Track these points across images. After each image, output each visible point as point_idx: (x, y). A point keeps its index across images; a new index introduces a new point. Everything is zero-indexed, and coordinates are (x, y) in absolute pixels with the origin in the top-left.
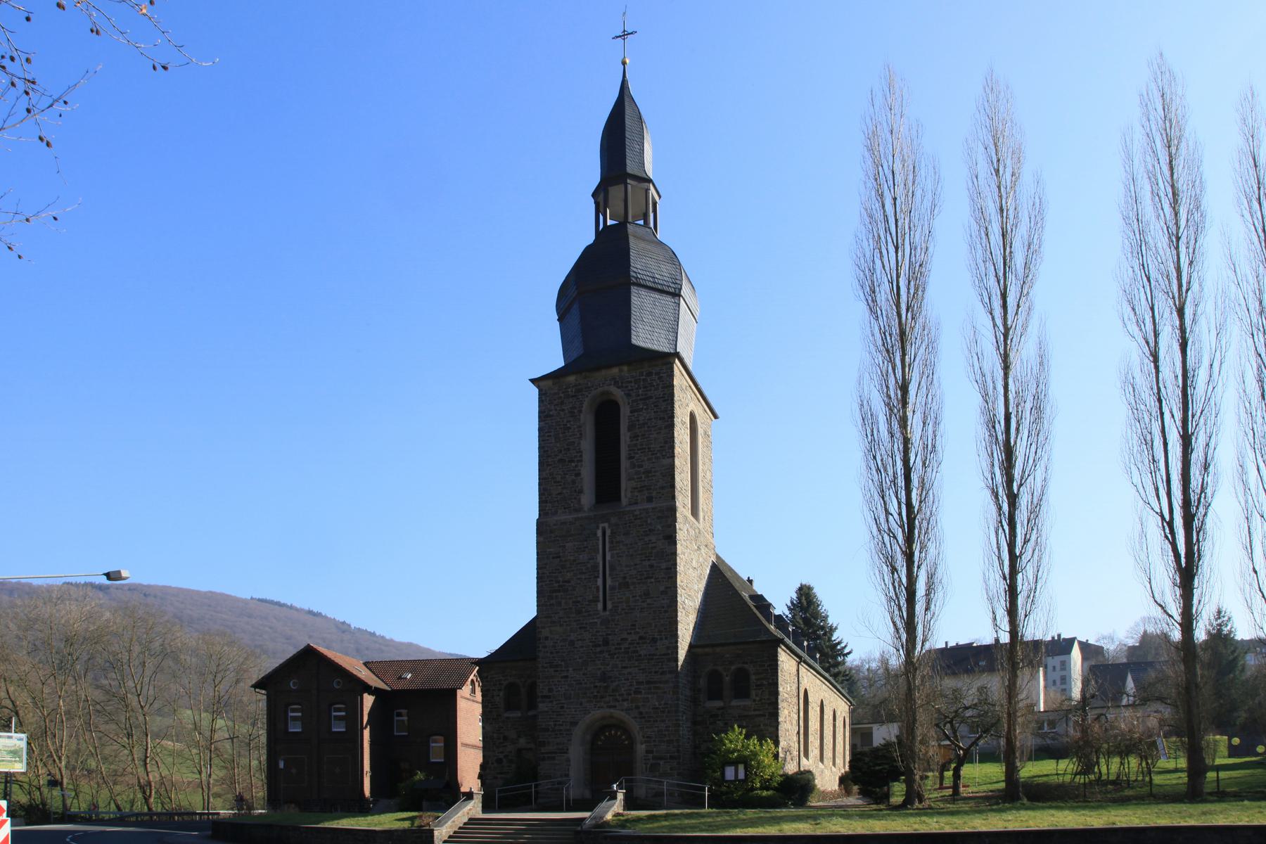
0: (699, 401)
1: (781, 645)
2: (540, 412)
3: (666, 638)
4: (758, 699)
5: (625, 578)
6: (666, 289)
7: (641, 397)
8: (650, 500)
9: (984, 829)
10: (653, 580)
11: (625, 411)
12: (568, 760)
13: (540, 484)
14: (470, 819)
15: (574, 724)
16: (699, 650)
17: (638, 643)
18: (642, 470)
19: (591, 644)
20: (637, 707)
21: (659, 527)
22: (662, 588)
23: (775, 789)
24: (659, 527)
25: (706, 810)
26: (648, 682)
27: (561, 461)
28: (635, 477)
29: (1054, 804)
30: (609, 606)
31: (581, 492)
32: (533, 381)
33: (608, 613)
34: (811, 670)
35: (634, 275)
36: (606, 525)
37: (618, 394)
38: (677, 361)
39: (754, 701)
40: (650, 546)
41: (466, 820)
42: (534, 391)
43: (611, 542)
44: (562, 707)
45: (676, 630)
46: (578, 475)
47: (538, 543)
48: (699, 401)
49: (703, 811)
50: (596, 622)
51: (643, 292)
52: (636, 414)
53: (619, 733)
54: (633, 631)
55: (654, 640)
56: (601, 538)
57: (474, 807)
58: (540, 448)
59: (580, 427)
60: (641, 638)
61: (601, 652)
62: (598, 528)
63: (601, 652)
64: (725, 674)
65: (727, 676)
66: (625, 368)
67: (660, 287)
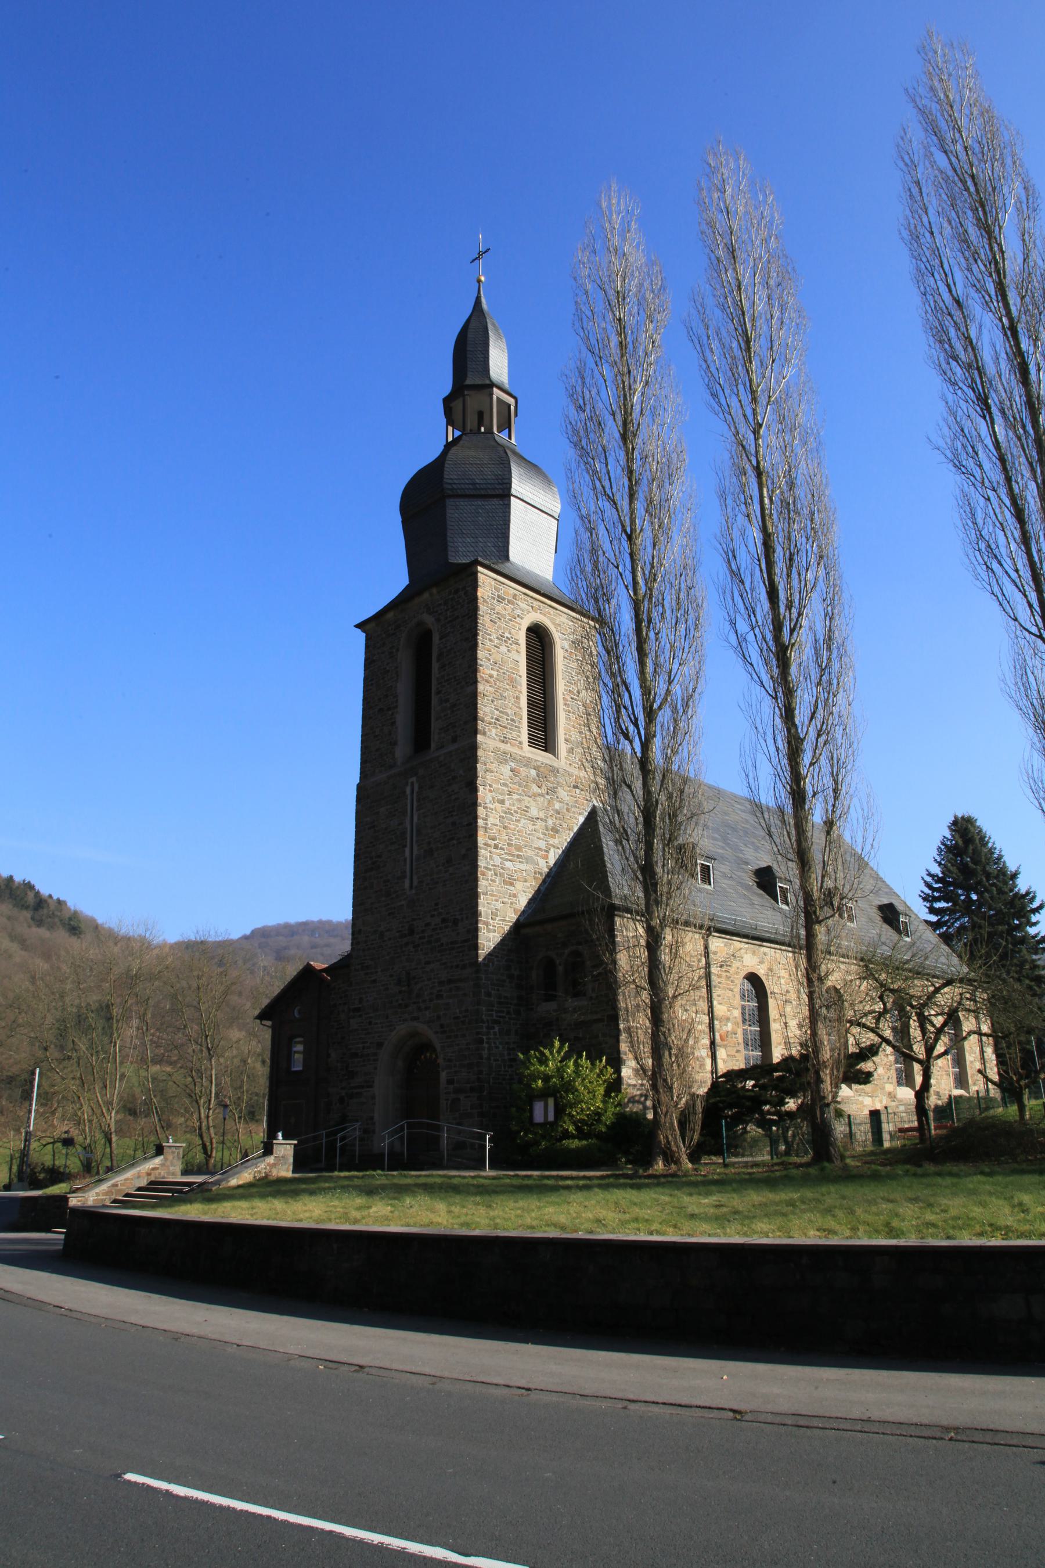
0: (556, 609)
1: (616, 913)
2: (366, 660)
3: (467, 918)
4: (594, 995)
5: (429, 843)
6: (490, 492)
7: (449, 619)
8: (454, 740)
9: (394, 1228)
10: (455, 842)
11: (436, 638)
12: (373, 1097)
13: (363, 742)
14: (151, 1183)
15: (380, 1045)
16: (525, 931)
17: (441, 929)
18: (448, 705)
19: (397, 934)
20: (439, 1017)
21: (461, 772)
22: (463, 851)
23: (599, 1136)
24: (461, 772)
25: (489, 1173)
26: (450, 981)
27: (381, 710)
28: (442, 715)
29: (437, 1176)
30: (415, 883)
31: (395, 743)
32: (358, 626)
33: (414, 891)
34: (765, 944)
35: (450, 487)
36: (414, 779)
37: (429, 620)
38: (480, 568)
39: (591, 998)
40: (453, 797)
41: (143, 1183)
42: (361, 637)
43: (418, 800)
44: (370, 1023)
45: (476, 905)
46: (393, 723)
47: (357, 813)
48: (556, 609)
49: (483, 1173)
50: (403, 905)
51: (462, 503)
52: (444, 640)
53: (428, 1055)
54: (436, 913)
55: (455, 922)
56: (409, 797)
57: (162, 1165)
58: (364, 700)
59: (397, 667)
60: (444, 920)
61: (407, 944)
62: (407, 784)
63: (407, 944)
64: (558, 962)
65: (560, 965)
66: (434, 591)
67: (483, 492)
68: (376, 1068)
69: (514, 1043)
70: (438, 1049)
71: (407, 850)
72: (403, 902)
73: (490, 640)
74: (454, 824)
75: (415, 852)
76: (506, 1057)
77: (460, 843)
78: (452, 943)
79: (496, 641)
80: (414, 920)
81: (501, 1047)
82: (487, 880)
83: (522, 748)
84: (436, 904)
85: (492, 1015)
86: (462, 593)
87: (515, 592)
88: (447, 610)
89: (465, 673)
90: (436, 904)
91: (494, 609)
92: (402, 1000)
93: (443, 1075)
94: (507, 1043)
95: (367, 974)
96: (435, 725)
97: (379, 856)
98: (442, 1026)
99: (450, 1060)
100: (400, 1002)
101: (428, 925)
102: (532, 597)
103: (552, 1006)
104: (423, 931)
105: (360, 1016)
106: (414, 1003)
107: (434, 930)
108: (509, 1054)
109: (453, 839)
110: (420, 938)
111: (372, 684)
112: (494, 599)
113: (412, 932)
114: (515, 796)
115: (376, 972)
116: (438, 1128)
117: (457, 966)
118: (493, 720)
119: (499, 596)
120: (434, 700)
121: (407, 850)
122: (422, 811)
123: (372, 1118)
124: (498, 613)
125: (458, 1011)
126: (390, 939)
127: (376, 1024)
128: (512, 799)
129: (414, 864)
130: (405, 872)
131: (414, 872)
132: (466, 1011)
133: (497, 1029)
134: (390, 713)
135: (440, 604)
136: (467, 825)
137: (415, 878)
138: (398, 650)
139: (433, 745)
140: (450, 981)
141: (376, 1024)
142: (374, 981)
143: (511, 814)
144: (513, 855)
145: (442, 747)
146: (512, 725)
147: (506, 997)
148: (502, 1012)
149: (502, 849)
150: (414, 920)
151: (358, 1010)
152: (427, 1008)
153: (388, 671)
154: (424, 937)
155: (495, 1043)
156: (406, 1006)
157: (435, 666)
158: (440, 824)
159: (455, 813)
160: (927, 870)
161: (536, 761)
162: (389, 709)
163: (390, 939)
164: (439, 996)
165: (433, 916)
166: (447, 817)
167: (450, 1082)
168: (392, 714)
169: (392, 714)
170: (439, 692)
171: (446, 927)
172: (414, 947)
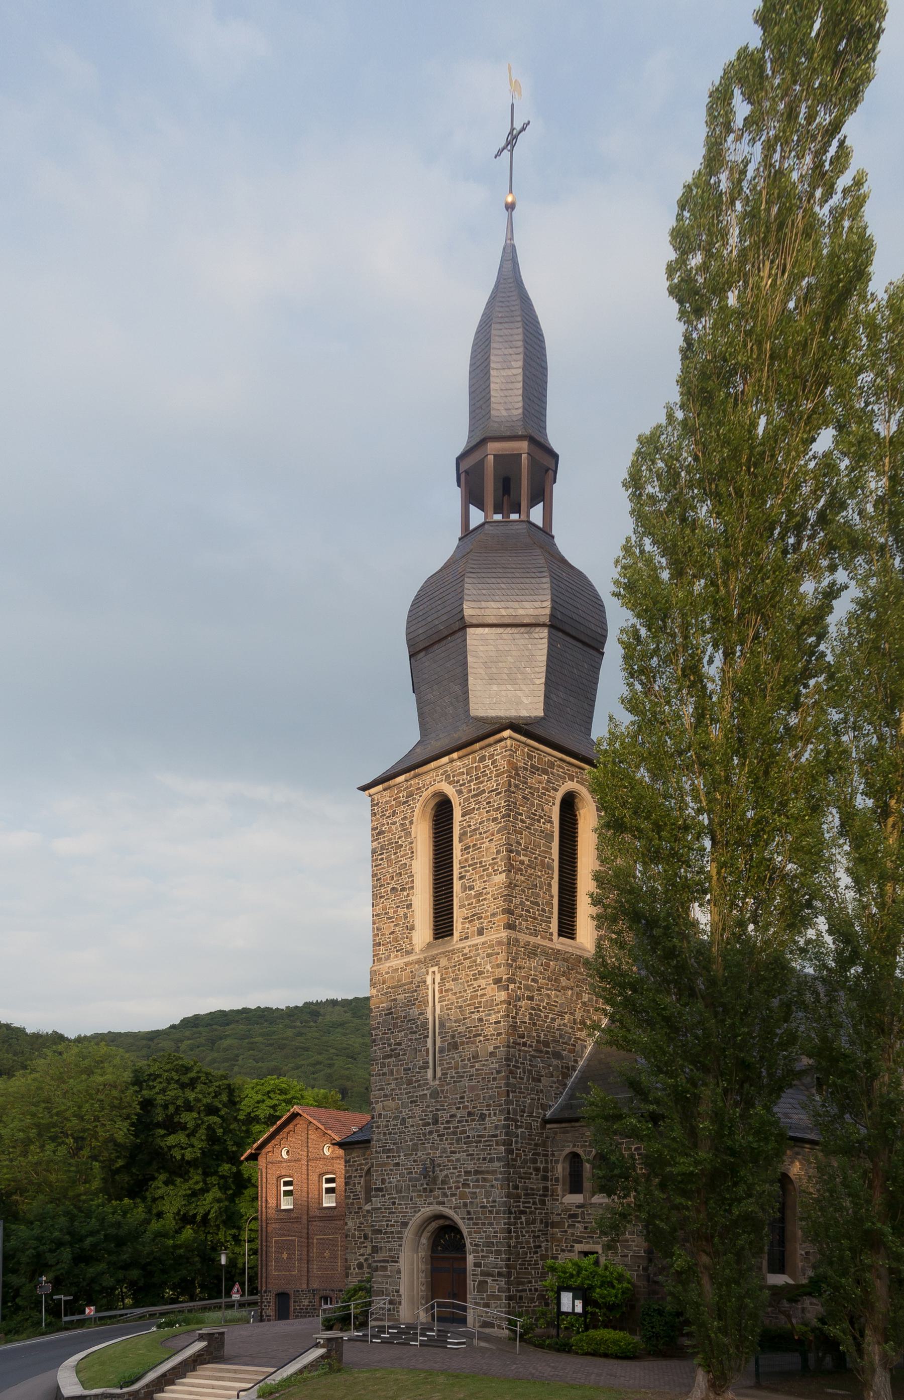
7: (473, 793)
8: (480, 932)
10: (482, 1038)
12: (399, 1272)
15: (405, 1224)
17: (467, 1121)
18: (473, 892)
20: (465, 1205)
21: (488, 967)
26: (477, 1172)
27: (393, 889)
28: (466, 903)
30: (439, 1074)
33: (437, 1082)
36: (436, 969)
40: (479, 993)
43: (441, 992)
44: (394, 1203)
46: (409, 906)
55: (483, 1117)
59: (412, 843)
60: (470, 1114)
61: (431, 1133)
63: (431, 1133)
68: (400, 1246)
69: (539, 1231)
70: (465, 1234)
71: (430, 1041)
72: (425, 1092)
73: (522, 821)
74: (480, 1020)
75: (438, 1044)
76: (532, 1245)
77: (488, 1040)
78: (478, 1136)
79: (528, 821)
80: (438, 1110)
81: (527, 1235)
82: (515, 1078)
83: (552, 940)
84: (462, 1098)
85: (519, 1206)
86: (488, 762)
87: (553, 759)
88: (469, 782)
89: (493, 859)
90: (462, 1098)
91: (526, 783)
92: (427, 1184)
93: (470, 1259)
94: (533, 1232)
95: (388, 1157)
96: (458, 914)
97: (399, 1044)
98: (469, 1213)
99: (476, 1245)
100: (425, 1186)
101: (452, 1116)
102: (569, 763)
103: (578, 1198)
104: (448, 1122)
105: (384, 1196)
106: (439, 1189)
107: (459, 1122)
108: (534, 1241)
109: (480, 1035)
110: (445, 1128)
111: (382, 859)
112: (526, 769)
113: (436, 1122)
114: (544, 991)
115: (399, 1156)
116: (464, 1309)
117: (484, 1159)
118: (524, 913)
119: (532, 766)
120: (457, 885)
121: (430, 1041)
122: (444, 1003)
123: (398, 1291)
124: (531, 788)
125: (485, 1200)
126: (412, 1126)
127: (401, 1204)
128: (541, 995)
129: (437, 1055)
130: (428, 1063)
131: (437, 1062)
132: (494, 1201)
133: (523, 1219)
134: (405, 893)
135: (463, 773)
136: (496, 1023)
137: (438, 1069)
138: (411, 822)
139: (456, 935)
140: (477, 1172)
141: (401, 1204)
142: (397, 1164)
143: (540, 1010)
144: (541, 1052)
145: (467, 938)
146: (543, 916)
147: (532, 1189)
148: (529, 1202)
149: (531, 1046)
150: (438, 1110)
151: (380, 1190)
152: (453, 1195)
153: (401, 846)
154: (449, 1128)
155: (522, 1232)
156: (431, 1191)
157: (457, 847)
158: (465, 1019)
159: (481, 1009)
160: (529, 122)
161: (566, 952)
162: (403, 890)
163: (412, 1126)
164: (466, 1185)
165: (459, 1108)
166: (473, 1012)
167: (477, 1265)
168: (408, 895)
169: (408, 895)
170: (461, 878)
171: (473, 1120)
172: (438, 1136)
